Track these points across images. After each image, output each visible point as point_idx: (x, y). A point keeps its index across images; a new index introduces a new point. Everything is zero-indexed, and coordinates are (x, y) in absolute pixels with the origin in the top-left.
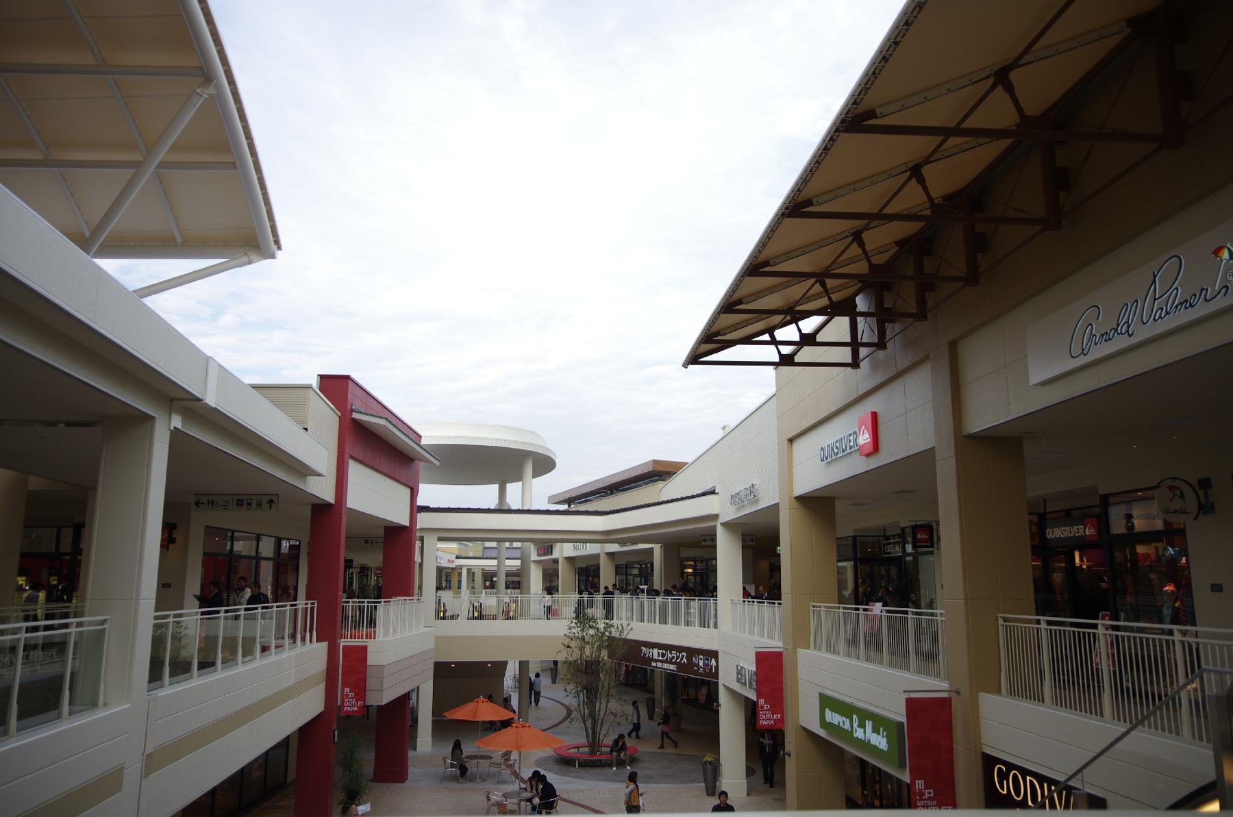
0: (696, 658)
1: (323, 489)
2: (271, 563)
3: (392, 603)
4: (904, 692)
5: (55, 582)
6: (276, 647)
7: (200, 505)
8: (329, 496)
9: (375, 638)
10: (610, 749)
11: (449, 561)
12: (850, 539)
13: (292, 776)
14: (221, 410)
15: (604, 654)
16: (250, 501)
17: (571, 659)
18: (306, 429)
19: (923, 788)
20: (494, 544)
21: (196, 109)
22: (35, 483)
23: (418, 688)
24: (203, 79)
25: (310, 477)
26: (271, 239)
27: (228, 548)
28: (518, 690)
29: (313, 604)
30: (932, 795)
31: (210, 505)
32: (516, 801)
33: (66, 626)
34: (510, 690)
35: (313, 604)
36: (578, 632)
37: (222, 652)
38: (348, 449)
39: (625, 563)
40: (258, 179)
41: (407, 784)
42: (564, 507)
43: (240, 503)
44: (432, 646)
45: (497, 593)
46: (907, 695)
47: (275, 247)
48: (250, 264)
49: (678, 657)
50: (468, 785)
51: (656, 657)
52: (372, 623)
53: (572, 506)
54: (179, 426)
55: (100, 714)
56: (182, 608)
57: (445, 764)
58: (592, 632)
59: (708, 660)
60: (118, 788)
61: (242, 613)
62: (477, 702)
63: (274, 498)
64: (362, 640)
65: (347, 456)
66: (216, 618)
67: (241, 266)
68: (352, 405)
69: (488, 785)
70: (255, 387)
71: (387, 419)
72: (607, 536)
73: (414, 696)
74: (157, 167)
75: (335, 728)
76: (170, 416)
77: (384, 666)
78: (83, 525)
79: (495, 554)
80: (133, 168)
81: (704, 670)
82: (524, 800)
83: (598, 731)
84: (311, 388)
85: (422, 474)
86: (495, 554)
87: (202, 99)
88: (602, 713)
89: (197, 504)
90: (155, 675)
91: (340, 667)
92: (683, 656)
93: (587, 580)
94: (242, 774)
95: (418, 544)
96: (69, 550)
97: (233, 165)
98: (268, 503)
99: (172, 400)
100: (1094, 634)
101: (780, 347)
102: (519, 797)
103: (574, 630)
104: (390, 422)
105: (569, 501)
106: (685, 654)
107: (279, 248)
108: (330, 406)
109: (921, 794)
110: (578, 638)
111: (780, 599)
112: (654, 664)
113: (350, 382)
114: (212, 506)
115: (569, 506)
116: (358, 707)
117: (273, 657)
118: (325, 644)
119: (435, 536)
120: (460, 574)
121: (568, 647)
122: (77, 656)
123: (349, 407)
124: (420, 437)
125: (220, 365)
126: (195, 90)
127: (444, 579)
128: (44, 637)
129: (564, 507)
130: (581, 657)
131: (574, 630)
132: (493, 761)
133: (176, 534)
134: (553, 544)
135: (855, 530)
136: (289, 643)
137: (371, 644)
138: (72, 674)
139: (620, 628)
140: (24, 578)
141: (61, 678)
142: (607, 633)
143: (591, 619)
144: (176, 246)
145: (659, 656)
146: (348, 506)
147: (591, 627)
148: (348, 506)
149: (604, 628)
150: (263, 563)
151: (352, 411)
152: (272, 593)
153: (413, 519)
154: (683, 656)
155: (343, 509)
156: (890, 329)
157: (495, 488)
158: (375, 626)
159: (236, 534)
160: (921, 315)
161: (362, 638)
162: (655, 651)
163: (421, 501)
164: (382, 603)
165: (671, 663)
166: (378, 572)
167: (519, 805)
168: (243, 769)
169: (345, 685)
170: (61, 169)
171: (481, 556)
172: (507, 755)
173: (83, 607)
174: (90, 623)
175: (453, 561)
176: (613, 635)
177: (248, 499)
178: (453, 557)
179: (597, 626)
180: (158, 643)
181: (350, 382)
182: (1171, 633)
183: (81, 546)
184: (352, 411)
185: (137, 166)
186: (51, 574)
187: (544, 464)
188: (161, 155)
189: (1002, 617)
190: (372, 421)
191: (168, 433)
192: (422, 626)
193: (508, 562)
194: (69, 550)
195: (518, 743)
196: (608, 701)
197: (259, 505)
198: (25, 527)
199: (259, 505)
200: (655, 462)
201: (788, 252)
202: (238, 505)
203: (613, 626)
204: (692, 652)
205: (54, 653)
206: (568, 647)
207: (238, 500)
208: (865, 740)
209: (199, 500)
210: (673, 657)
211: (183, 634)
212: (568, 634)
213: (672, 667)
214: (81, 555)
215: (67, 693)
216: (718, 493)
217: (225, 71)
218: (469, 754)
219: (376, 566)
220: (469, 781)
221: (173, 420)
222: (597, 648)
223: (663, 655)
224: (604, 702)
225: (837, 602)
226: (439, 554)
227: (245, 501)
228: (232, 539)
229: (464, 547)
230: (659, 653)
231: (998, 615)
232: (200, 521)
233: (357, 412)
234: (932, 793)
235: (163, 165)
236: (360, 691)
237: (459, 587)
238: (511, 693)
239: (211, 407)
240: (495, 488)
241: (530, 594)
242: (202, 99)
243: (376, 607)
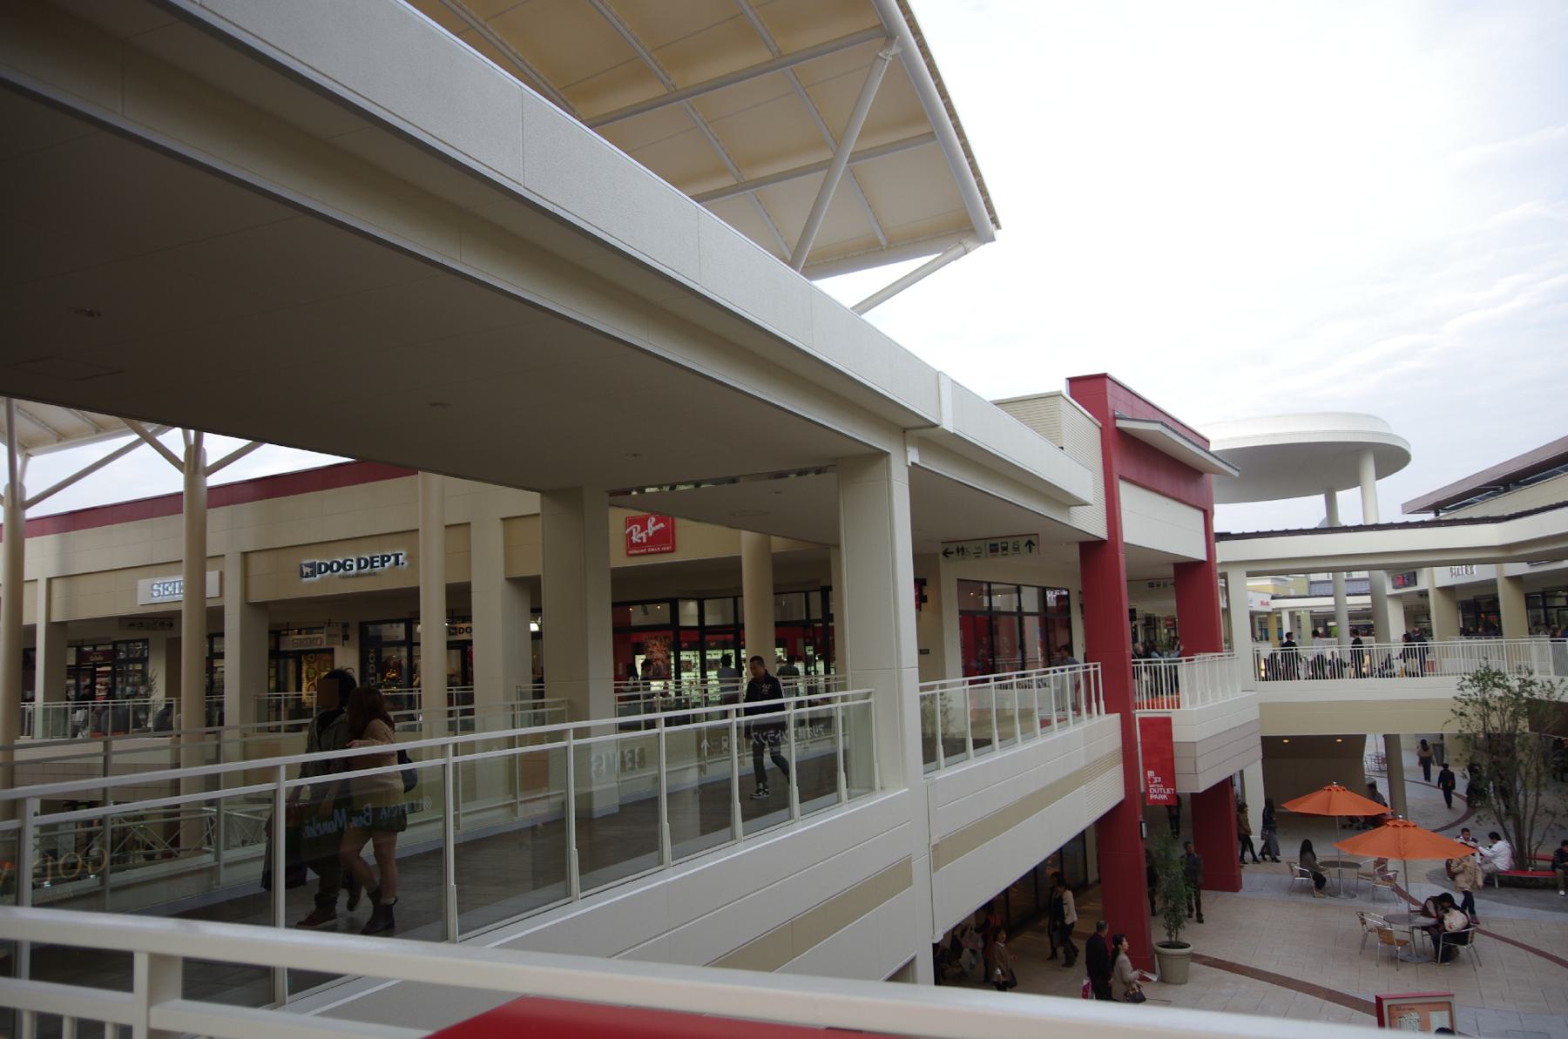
1: (1092, 522)
2: (1036, 619)
3: (1196, 661)
5: (811, 653)
6: (1059, 721)
8: (1099, 530)
9: (1179, 707)
10: (1550, 864)
11: (1262, 603)
13: (1093, 876)
14: (962, 435)
15: (1524, 724)
16: (1005, 545)
17: (1467, 731)
18: (1062, 448)
20: (1323, 576)
21: (881, 78)
22: (778, 544)
23: (1241, 772)
24: (884, 39)
25: (1074, 508)
26: (988, 218)
27: (986, 604)
28: (1386, 775)
29: (1095, 666)
31: (960, 553)
32: (1406, 928)
33: (781, 707)
34: (1371, 773)
35: (1095, 666)
36: (1475, 694)
37: (998, 728)
38: (1117, 469)
39: (1540, 590)
40: (962, 145)
41: (1241, 893)
42: (1430, 516)
43: (994, 549)
44: (1256, 715)
47: (992, 227)
48: (966, 253)
50: (1328, 900)
52: (1174, 685)
53: (1441, 514)
54: (917, 461)
55: (879, 799)
56: (944, 678)
57: (1292, 871)
58: (1498, 692)
60: (908, 882)
61: (791, 713)
62: (1329, 790)
63: (1033, 539)
64: (1163, 710)
65: (1116, 476)
66: (986, 687)
67: (956, 258)
68: (1114, 411)
69: (1359, 903)
70: (999, 404)
71: (1162, 423)
72: (1509, 552)
73: (1237, 781)
74: (848, 163)
75: (1141, 820)
76: (906, 452)
77: (1194, 743)
78: (830, 588)
79: (1329, 589)
80: (821, 169)
82: (1418, 928)
83: (1527, 837)
84: (1061, 395)
85: (1216, 492)
86: (1329, 589)
87: (887, 63)
88: (1531, 810)
89: (946, 553)
90: (929, 756)
91: (1139, 745)
93: (1478, 618)
94: (1036, 872)
95: (1221, 583)
96: (820, 617)
97: (931, 136)
99: (905, 430)
102: (1410, 923)
103: (1467, 691)
104: (1167, 426)
105: (1437, 507)
107: (998, 227)
108: (1086, 416)
109: (1152, 780)
110: (1476, 702)
113: (1108, 381)
115: (1437, 514)
116: (1168, 795)
117: (1057, 734)
118: (1116, 717)
119: (1242, 572)
120: (1280, 620)
121: (1462, 714)
122: (847, 732)
123: (1110, 414)
124: (1208, 441)
125: (953, 381)
126: (877, 56)
127: (1257, 626)
128: (810, 712)
129: (1430, 516)
130: (1484, 729)
131: (1467, 691)
132: (1361, 870)
133: (926, 591)
134: (1417, 570)
136: (1073, 715)
137: (1175, 714)
138: (845, 752)
139: (1548, 686)
140: (781, 649)
141: (834, 756)
142: (1525, 695)
143: (1496, 674)
144: (882, 250)
147: (1495, 685)
149: (1520, 686)
150: (1027, 619)
151: (1115, 418)
152: (1042, 655)
153: (1210, 550)
155: (1120, 545)
157: (1319, 500)
158: (1178, 691)
159: (994, 587)
161: (1163, 707)
163: (1219, 526)
164: (1184, 662)
166: (1168, 623)
167: (1411, 933)
168: (1035, 869)
169: (1147, 767)
170: (754, 190)
171: (1307, 594)
172: (1381, 863)
173: (845, 679)
174: (854, 698)
175: (1267, 604)
176: (1536, 697)
177: (1002, 543)
178: (1267, 598)
179: (1507, 684)
180: (927, 717)
181: (1108, 381)
182: (1160, 662)
183: (831, 612)
184: (1115, 418)
185: (828, 165)
186: (806, 645)
187: (1392, 459)
188: (851, 146)
190: (1151, 428)
192: (1239, 689)
193: (1351, 600)
194: (820, 617)
195: (1399, 848)
196: (1538, 795)
197: (1017, 549)
198: (775, 594)
199: (1017, 549)
202: (991, 551)
203: (1535, 684)
205: (821, 730)
206: (1462, 714)
207: (991, 545)
209: (947, 549)
211: (948, 707)
212: (1459, 697)
214: (832, 621)
215: (842, 775)
217: (907, 21)
218: (1324, 860)
219: (1165, 616)
220: (1330, 895)
221: (909, 455)
222: (1511, 716)
224: (1532, 794)
226: (1251, 595)
228: (990, 594)
229: (1279, 583)
232: (950, 573)
233: (1121, 419)
235: (855, 157)
236: (1169, 777)
238: (1376, 779)
239: (950, 433)
240: (1319, 500)
241: (1389, 641)
242: (887, 63)
243: (1176, 667)
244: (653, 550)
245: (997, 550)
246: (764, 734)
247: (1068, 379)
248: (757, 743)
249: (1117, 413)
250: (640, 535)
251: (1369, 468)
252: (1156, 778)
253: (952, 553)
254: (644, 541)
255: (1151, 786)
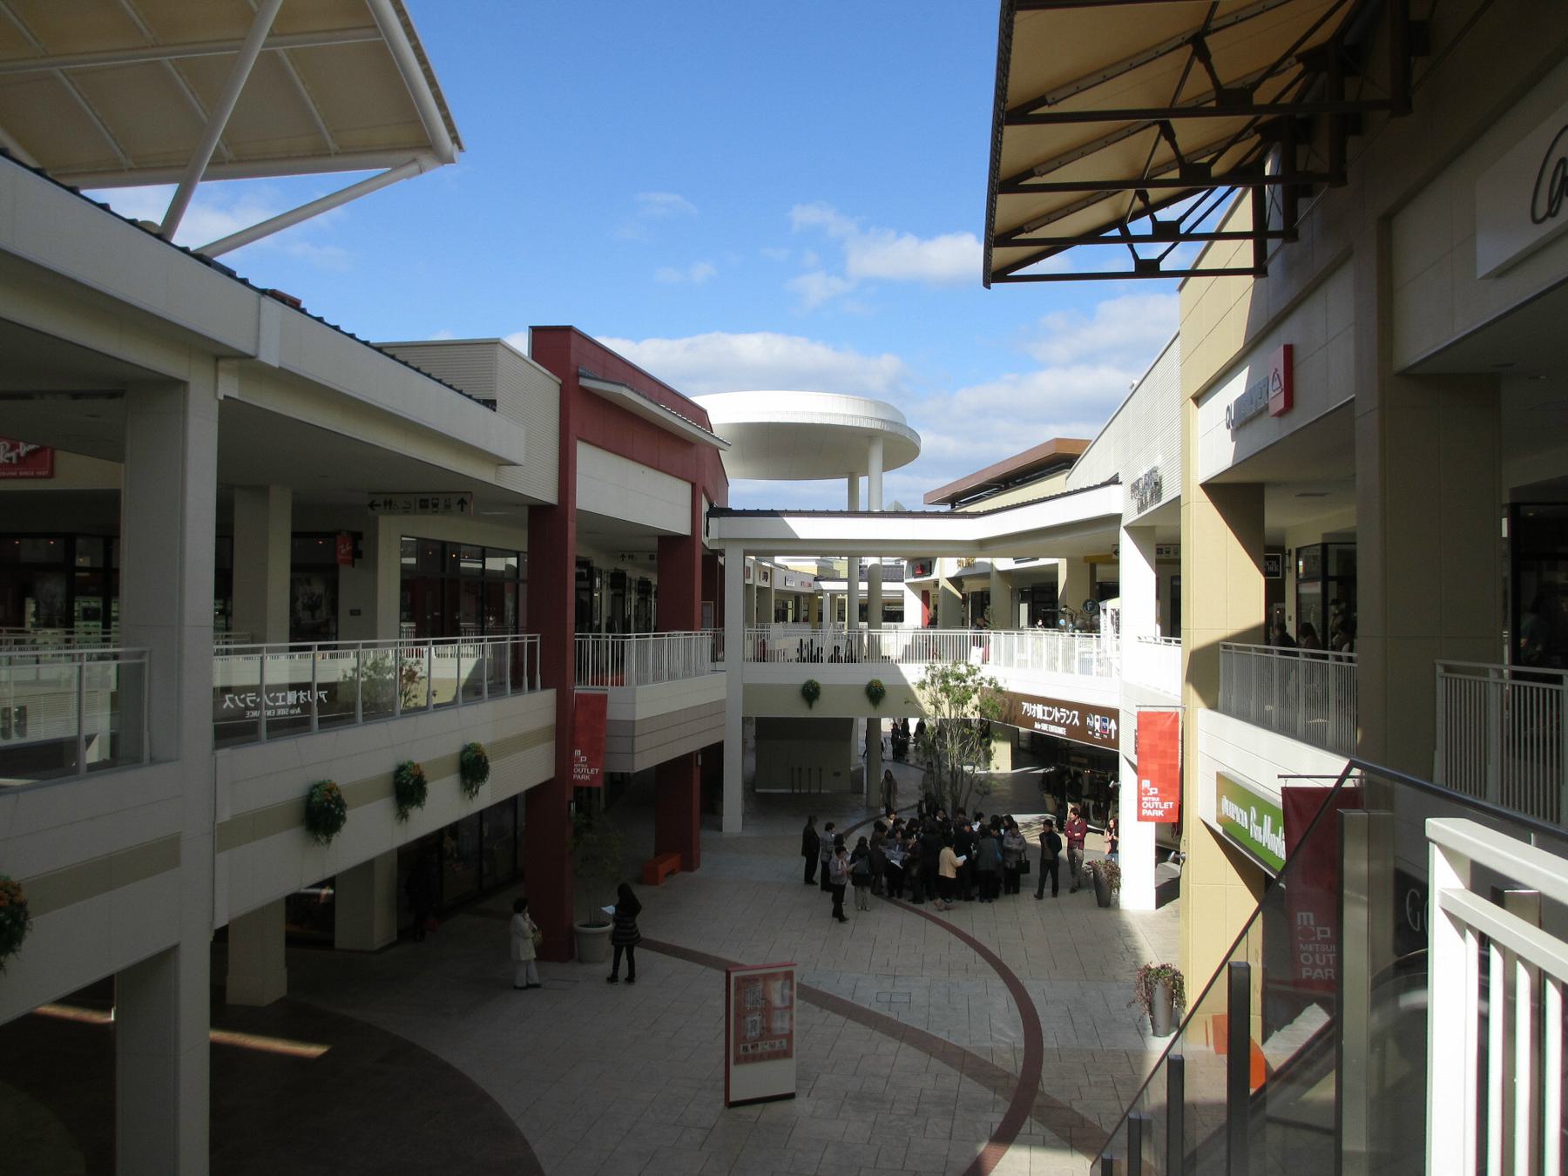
0: (1091, 720)
4: (1280, 777)
7: (375, 508)
8: (546, 493)
12: (1319, 547)
19: (1312, 923)
30: (1329, 935)
31: (388, 507)
43: (424, 505)
45: (923, 628)
46: (1282, 783)
48: (421, 172)
49: (1068, 717)
51: (1040, 716)
54: (234, 394)
59: (1105, 721)
63: (467, 498)
67: (409, 176)
68: (578, 367)
81: (1101, 735)
92: (1074, 715)
98: (373, 509)
100: (1558, 691)
101: (1136, 245)
106: (1076, 713)
111: (1179, 635)
112: (1037, 726)
113: (573, 336)
114: (390, 509)
115: (953, 506)
118: (550, 694)
129: (947, 508)
135: (1324, 535)
137: (612, 692)
145: (1044, 715)
146: (577, 507)
148: (577, 507)
154: (1074, 715)
156: (1304, 205)
160: (1338, 177)
162: (1039, 708)
165: (1059, 724)
177: (433, 499)
182: (588, 637)
184: (578, 376)
189: (1440, 664)
191: (216, 406)
197: (448, 507)
199: (448, 507)
200: (1058, 441)
201: (1078, 80)
202: (421, 507)
204: (1086, 710)
207: (421, 500)
208: (1262, 844)
209: (374, 501)
210: (1062, 717)
213: (1061, 731)
216: (1121, 483)
223: (1050, 714)
225: (1263, 640)
227: (430, 501)
230: (1044, 711)
231: (1436, 661)
234: (1329, 932)
237: (821, 619)
244: (26, 473)
245: (427, 507)
246: (242, 697)
247: (530, 327)
248: (232, 706)
249: (580, 370)
250: (8, 455)
251: (876, 461)
252: (1152, 789)
253: (379, 505)
254: (14, 461)
255: (1144, 799)
